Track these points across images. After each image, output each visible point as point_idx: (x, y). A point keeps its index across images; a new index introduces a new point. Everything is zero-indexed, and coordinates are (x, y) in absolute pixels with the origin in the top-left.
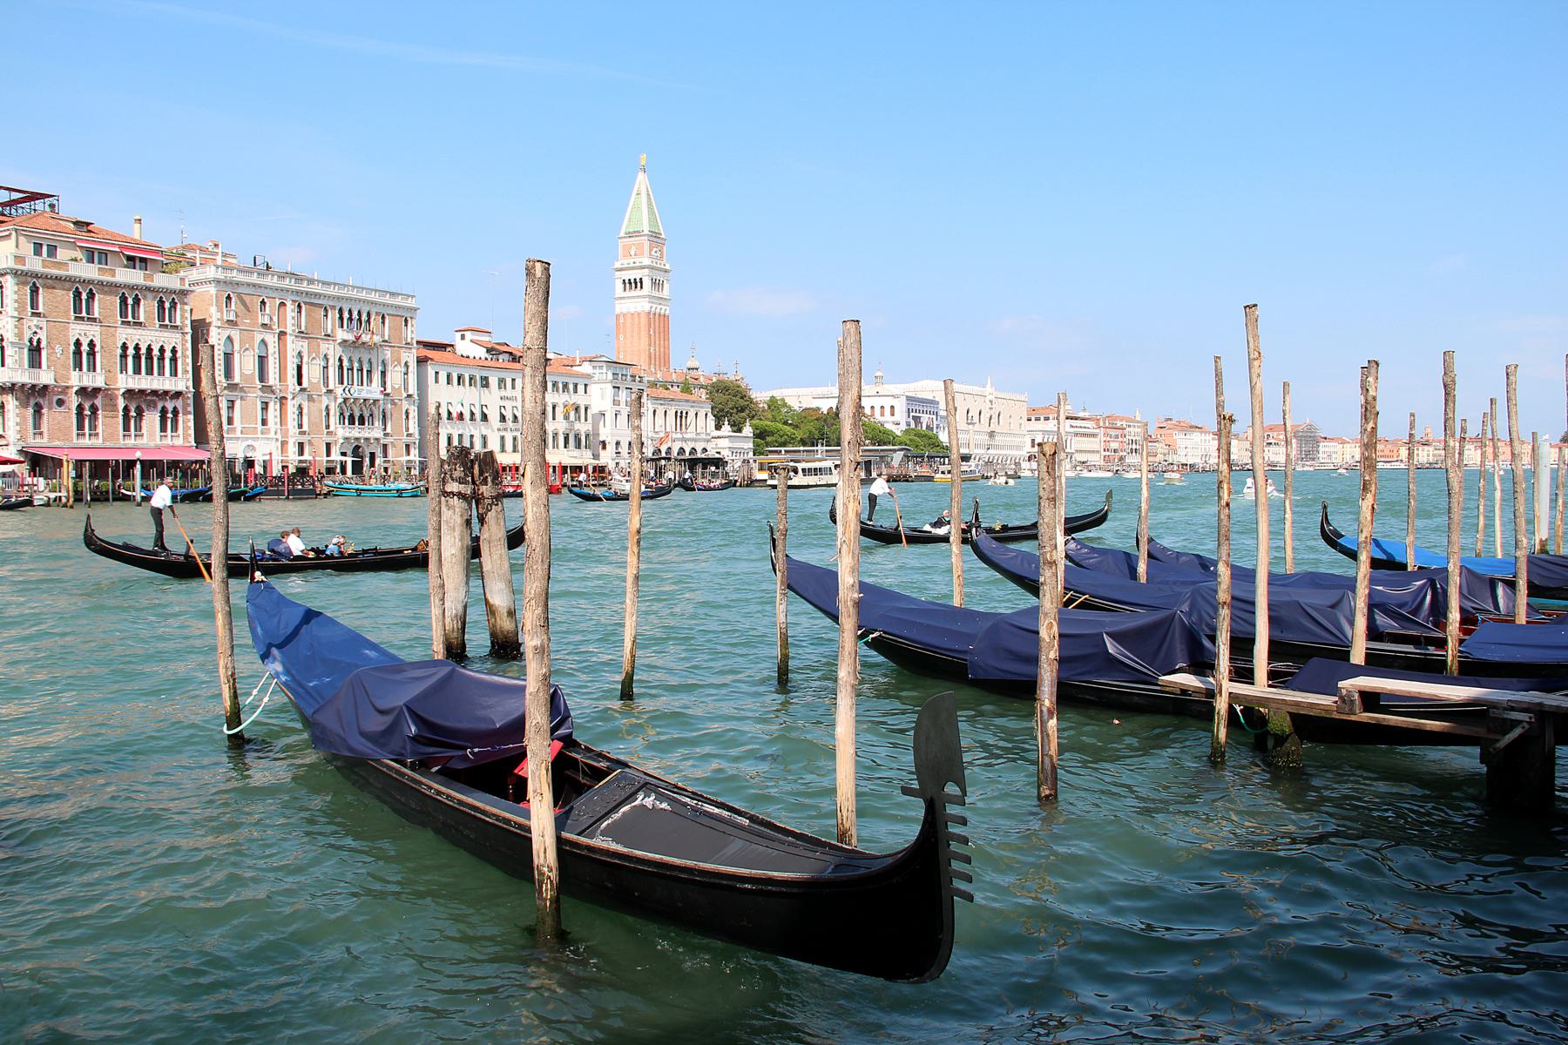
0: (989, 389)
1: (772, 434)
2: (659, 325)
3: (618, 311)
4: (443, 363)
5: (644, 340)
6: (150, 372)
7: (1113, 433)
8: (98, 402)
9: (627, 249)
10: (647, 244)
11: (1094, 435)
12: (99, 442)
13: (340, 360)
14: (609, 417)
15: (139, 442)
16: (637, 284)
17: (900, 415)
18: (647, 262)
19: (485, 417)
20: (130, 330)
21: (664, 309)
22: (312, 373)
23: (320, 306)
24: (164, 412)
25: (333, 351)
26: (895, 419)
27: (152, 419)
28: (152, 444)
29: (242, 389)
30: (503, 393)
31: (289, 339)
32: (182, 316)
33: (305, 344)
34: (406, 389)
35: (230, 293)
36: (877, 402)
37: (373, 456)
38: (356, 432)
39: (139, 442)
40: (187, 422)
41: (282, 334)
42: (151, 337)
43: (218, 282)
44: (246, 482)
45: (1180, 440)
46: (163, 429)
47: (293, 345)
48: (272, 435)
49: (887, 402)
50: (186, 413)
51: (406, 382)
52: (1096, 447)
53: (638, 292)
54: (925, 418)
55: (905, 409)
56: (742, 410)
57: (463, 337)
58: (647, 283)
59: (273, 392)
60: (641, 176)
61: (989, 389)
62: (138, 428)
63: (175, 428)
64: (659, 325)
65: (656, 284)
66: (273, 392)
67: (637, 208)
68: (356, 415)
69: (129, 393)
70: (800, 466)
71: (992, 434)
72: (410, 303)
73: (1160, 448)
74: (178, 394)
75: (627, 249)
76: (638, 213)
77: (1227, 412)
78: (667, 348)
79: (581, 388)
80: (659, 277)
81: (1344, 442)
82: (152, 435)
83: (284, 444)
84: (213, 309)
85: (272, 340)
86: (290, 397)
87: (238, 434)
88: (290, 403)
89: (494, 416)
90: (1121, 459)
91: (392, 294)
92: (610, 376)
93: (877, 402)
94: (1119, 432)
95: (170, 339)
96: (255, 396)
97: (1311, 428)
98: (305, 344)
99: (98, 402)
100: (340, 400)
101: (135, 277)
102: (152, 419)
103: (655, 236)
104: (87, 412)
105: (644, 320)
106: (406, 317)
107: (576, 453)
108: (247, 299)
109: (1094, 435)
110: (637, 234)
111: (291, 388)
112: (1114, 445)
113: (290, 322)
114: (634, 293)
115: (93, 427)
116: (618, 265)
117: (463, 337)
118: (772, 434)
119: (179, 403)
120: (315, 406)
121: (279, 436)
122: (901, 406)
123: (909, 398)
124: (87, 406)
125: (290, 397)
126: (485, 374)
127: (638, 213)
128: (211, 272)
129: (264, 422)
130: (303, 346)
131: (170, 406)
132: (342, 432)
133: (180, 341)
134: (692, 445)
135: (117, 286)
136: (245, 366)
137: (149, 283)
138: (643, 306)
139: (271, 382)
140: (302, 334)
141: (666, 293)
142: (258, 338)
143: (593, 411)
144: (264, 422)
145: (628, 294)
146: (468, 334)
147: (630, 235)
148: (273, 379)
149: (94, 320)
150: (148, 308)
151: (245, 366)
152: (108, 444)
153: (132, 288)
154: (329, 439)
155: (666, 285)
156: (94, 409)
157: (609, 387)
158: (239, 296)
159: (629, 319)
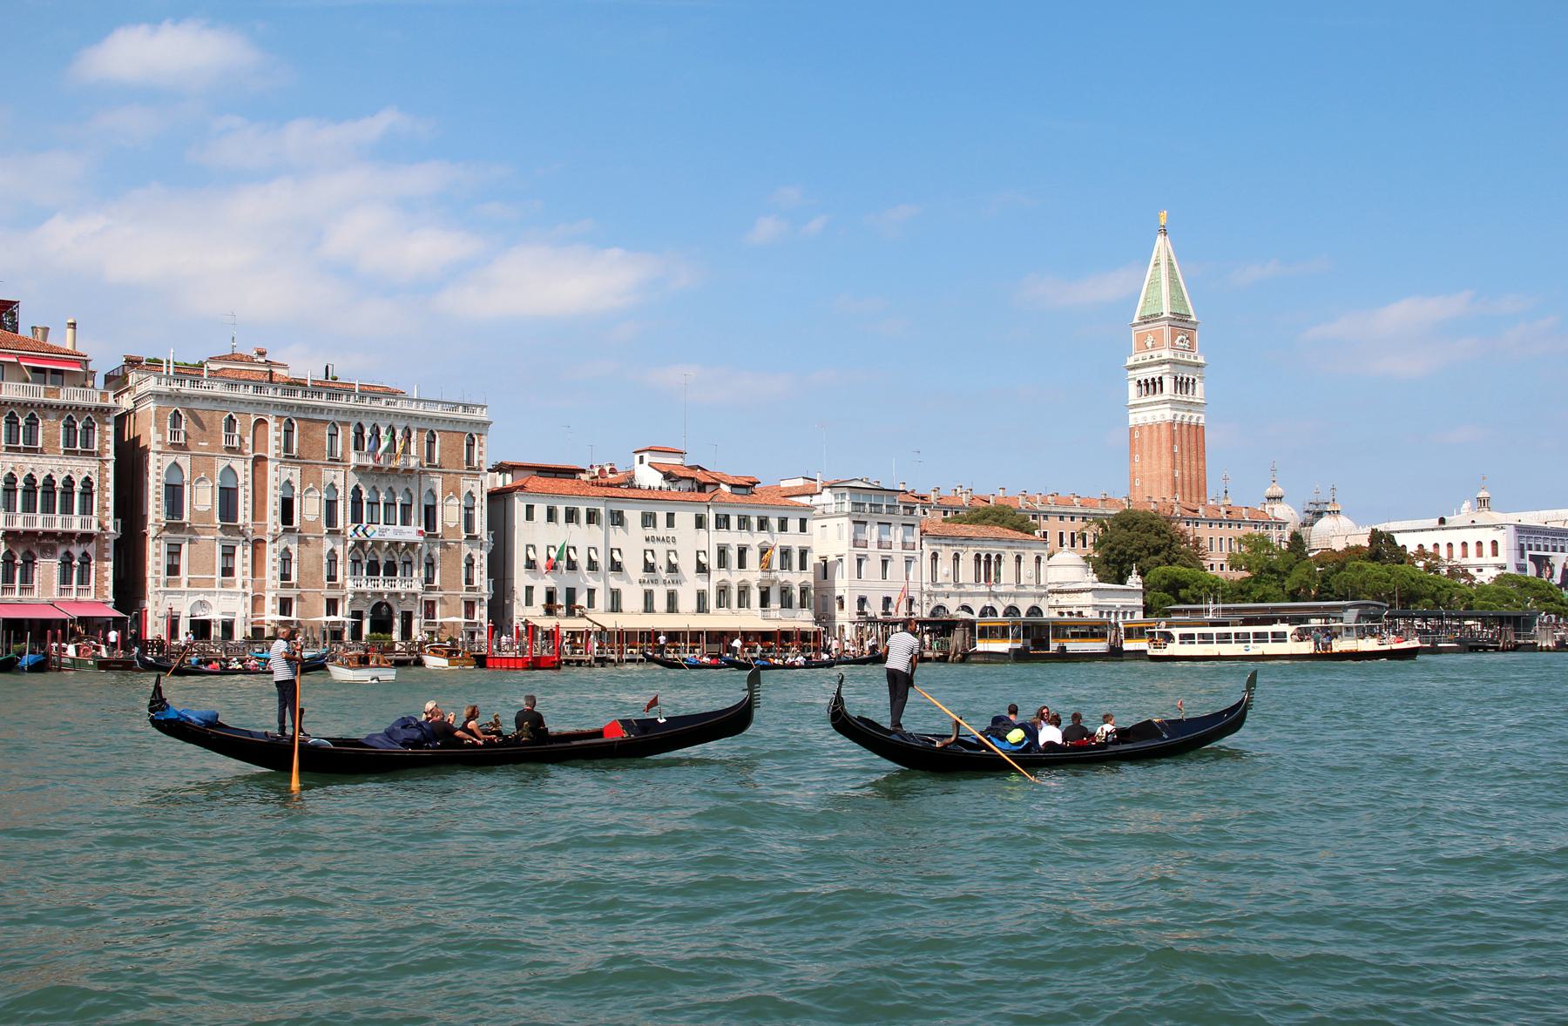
1: (1185, 585)
2: (1188, 441)
3: (1132, 423)
4: (541, 494)
5: (1166, 461)
9: (1142, 338)
10: (1167, 331)
14: (849, 565)
15: (26, 597)
16: (1153, 385)
17: (1507, 557)
18: (1167, 354)
19: (616, 567)
20: (19, 459)
21: (1195, 417)
22: (309, 509)
23: (326, 422)
25: (343, 481)
26: (1500, 560)
28: (45, 599)
29: (192, 530)
30: (650, 532)
31: (271, 466)
32: (102, 440)
33: (297, 472)
37: (407, 617)
38: (382, 585)
39: (26, 597)
40: (105, 572)
41: (259, 461)
42: (52, 466)
44: (406, 632)
46: (65, 579)
47: (275, 475)
48: (239, 587)
49: (1487, 536)
50: (101, 558)
51: (469, 520)
55: (1513, 543)
56: (1157, 551)
57: (641, 461)
58: (1168, 383)
59: (242, 533)
60: (1160, 239)
62: (27, 578)
63: (83, 580)
64: (1188, 441)
65: (1182, 384)
66: (242, 533)
67: (1155, 283)
70: (1176, 632)
72: (479, 415)
74: (87, 538)
75: (1142, 338)
76: (1157, 290)
77: (709, 489)
78: (1201, 471)
79: (794, 524)
82: (47, 587)
85: (242, 468)
86: (269, 539)
87: (184, 586)
88: (269, 548)
91: (466, 407)
92: (847, 507)
93: (1471, 536)
95: (81, 468)
96: (212, 541)
98: (297, 472)
100: (350, 544)
102: (47, 569)
103: (1180, 320)
104: (19, 561)
105: (1165, 433)
106: (471, 434)
108: (205, 417)
111: (271, 528)
114: (1151, 398)
116: (1131, 362)
117: (641, 461)
118: (1185, 585)
119: (91, 548)
120: (309, 552)
121: (249, 589)
122: (1506, 540)
123: (1521, 530)
126: (616, 507)
130: (295, 474)
131: (77, 551)
132: (349, 584)
133: (101, 472)
136: (202, 499)
137: (53, 400)
138: (1165, 414)
139: (477, 532)
140: (288, 456)
141: (1199, 393)
142: (221, 465)
143: (813, 559)
146: (646, 456)
147: (1146, 320)
148: (244, 516)
149: (92, 454)
151: (202, 499)
153: (25, 406)
154: (333, 594)
155: (1199, 385)
157: (846, 522)
158: (190, 412)
159: (1146, 433)
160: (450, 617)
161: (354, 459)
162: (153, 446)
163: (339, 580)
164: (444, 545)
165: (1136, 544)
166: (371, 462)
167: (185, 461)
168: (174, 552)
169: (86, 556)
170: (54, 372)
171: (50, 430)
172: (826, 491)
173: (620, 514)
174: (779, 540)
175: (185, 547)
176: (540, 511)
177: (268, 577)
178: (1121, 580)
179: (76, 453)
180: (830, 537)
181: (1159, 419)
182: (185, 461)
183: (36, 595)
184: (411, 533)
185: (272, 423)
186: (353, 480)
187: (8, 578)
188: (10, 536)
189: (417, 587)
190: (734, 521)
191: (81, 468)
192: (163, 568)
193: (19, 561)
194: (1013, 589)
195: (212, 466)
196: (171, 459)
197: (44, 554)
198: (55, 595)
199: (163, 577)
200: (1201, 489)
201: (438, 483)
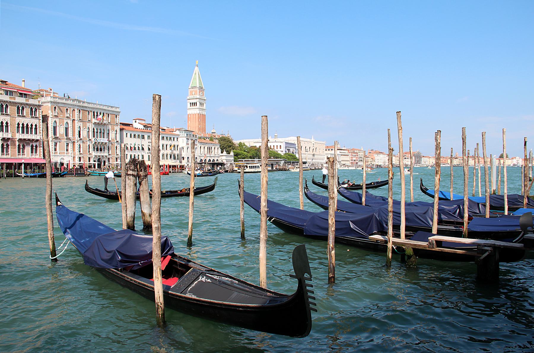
0: (313, 140)
1: (240, 155)
2: (202, 118)
3: (188, 113)
5: (197, 123)
6: (27, 133)
7: (354, 154)
8: (9, 143)
9: (191, 92)
11: (348, 155)
12: (9, 156)
13: (94, 129)
14: (185, 149)
15: (23, 157)
16: (195, 104)
17: (283, 149)
18: (198, 97)
19: (143, 149)
20: (20, 118)
21: (204, 113)
22: (84, 134)
23: (87, 111)
24: (32, 146)
25: (91, 126)
27: (28, 149)
28: (28, 158)
29: (59, 139)
34: (116, 139)
35: (55, 106)
36: (275, 144)
37: (105, 162)
38: (99, 154)
39: (23, 157)
41: (74, 120)
42: (28, 121)
43: (51, 102)
45: (376, 157)
46: (32, 152)
47: (77, 124)
48: (70, 154)
49: (279, 144)
50: (40, 147)
51: (116, 137)
52: (348, 159)
53: (195, 107)
54: (291, 150)
56: (230, 147)
57: (136, 122)
58: (198, 104)
59: (70, 140)
60: (196, 68)
61: (313, 140)
62: (23, 152)
63: (36, 152)
64: (202, 118)
65: (201, 104)
66: (70, 140)
67: (195, 79)
68: (99, 148)
69: (20, 140)
71: (314, 155)
72: (118, 110)
73: (370, 159)
74: (37, 140)
75: (191, 92)
79: (176, 139)
80: (202, 102)
81: (430, 158)
83: (74, 157)
84: (50, 112)
85: (70, 122)
86: (76, 142)
87: (58, 154)
88: (76, 144)
89: (146, 149)
90: (357, 163)
91: (112, 107)
92: (186, 135)
93: (275, 144)
94: (356, 154)
95: (35, 122)
96: (64, 141)
97: (419, 153)
99: (9, 143)
100: (93, 143)
101: (22, 100)
102: (28, 149)
103: (201, 88)
104: (21, 147)
105: (197, 116)
107: (174, 161)
109: (348, 155)
110: (195, 87)
111: (76, 139)
112: (354, 159)
113: (76, 116)
114: (193, 107)
115: (7, 151)
116: (188, 98)
117: (136, 122)
118: (240, 155)
119: (38, 144)
121: (72, 155)
122: (283, 145)
124: (5, 144)
125: (76, 142)
127: (195, 80)
128: (49, 99)
129: (67, 150)
132: (94, 154)
134: (217, 158)
135: (16, 103)
136: (61, 131)
137: (27, 102)
138: (197, 111)
139: (70, 137)
140: (80, 120)
141: (204, 107)
142: (65, 121)
143: (180, 147)
144: (67, 150)
145: (192, 107)
146: (137, 121)
147: (192, 88)
148: (70, 135)
149: (8, 115)
150: (27, 111)
151: (61, 131)
152: (12, 157)
153: (21, 104)
154: (90, 156)
155: (205, 105)
156: (8, 145)
157: (185, 139)
160: (113, 162)
161: (94, 121)
162: (50, 116)
163: (91, 152)
164: (112, 144)
165: (226, 145)
166: (97, 121)
167: (57, 120)
168: (56, 145)
169: (36, 146)
170: (25, 94)
171: (27, 111)
172: (177, 131)
173: (143, 136)
174: (173, 143)
175: (58, 144)
176: (129, 135)
177: (76, 151)
178: (229, 154)
179: (4, 114)
180: (182, 142)
181: (195, 113)
182: (57, 120)
183: (25, 156)
184: (105, 140)
185: (76, 111)
186: (93, 126)
187: (3, 151)
188: (3, 139)
189: (107, 154)
190: (165, 138)
191: (35, 122)
192: (54, 149)
193: (21, 147)
194: (213, 155)
195: (63, 122)
196: (54, 120)
197: (27, 144)
198: (30, 157)
199: (54, 152)
200: (205, 131)
201: (110, 127)
